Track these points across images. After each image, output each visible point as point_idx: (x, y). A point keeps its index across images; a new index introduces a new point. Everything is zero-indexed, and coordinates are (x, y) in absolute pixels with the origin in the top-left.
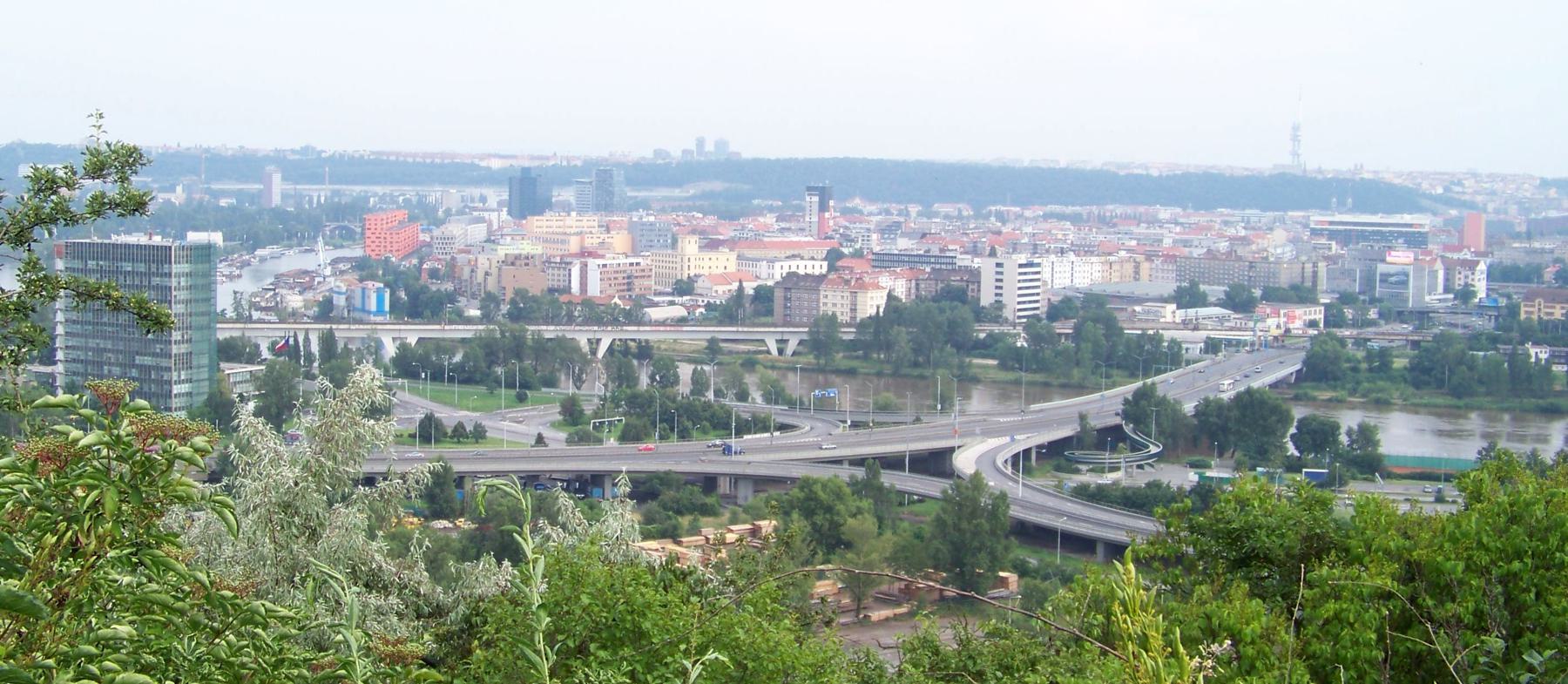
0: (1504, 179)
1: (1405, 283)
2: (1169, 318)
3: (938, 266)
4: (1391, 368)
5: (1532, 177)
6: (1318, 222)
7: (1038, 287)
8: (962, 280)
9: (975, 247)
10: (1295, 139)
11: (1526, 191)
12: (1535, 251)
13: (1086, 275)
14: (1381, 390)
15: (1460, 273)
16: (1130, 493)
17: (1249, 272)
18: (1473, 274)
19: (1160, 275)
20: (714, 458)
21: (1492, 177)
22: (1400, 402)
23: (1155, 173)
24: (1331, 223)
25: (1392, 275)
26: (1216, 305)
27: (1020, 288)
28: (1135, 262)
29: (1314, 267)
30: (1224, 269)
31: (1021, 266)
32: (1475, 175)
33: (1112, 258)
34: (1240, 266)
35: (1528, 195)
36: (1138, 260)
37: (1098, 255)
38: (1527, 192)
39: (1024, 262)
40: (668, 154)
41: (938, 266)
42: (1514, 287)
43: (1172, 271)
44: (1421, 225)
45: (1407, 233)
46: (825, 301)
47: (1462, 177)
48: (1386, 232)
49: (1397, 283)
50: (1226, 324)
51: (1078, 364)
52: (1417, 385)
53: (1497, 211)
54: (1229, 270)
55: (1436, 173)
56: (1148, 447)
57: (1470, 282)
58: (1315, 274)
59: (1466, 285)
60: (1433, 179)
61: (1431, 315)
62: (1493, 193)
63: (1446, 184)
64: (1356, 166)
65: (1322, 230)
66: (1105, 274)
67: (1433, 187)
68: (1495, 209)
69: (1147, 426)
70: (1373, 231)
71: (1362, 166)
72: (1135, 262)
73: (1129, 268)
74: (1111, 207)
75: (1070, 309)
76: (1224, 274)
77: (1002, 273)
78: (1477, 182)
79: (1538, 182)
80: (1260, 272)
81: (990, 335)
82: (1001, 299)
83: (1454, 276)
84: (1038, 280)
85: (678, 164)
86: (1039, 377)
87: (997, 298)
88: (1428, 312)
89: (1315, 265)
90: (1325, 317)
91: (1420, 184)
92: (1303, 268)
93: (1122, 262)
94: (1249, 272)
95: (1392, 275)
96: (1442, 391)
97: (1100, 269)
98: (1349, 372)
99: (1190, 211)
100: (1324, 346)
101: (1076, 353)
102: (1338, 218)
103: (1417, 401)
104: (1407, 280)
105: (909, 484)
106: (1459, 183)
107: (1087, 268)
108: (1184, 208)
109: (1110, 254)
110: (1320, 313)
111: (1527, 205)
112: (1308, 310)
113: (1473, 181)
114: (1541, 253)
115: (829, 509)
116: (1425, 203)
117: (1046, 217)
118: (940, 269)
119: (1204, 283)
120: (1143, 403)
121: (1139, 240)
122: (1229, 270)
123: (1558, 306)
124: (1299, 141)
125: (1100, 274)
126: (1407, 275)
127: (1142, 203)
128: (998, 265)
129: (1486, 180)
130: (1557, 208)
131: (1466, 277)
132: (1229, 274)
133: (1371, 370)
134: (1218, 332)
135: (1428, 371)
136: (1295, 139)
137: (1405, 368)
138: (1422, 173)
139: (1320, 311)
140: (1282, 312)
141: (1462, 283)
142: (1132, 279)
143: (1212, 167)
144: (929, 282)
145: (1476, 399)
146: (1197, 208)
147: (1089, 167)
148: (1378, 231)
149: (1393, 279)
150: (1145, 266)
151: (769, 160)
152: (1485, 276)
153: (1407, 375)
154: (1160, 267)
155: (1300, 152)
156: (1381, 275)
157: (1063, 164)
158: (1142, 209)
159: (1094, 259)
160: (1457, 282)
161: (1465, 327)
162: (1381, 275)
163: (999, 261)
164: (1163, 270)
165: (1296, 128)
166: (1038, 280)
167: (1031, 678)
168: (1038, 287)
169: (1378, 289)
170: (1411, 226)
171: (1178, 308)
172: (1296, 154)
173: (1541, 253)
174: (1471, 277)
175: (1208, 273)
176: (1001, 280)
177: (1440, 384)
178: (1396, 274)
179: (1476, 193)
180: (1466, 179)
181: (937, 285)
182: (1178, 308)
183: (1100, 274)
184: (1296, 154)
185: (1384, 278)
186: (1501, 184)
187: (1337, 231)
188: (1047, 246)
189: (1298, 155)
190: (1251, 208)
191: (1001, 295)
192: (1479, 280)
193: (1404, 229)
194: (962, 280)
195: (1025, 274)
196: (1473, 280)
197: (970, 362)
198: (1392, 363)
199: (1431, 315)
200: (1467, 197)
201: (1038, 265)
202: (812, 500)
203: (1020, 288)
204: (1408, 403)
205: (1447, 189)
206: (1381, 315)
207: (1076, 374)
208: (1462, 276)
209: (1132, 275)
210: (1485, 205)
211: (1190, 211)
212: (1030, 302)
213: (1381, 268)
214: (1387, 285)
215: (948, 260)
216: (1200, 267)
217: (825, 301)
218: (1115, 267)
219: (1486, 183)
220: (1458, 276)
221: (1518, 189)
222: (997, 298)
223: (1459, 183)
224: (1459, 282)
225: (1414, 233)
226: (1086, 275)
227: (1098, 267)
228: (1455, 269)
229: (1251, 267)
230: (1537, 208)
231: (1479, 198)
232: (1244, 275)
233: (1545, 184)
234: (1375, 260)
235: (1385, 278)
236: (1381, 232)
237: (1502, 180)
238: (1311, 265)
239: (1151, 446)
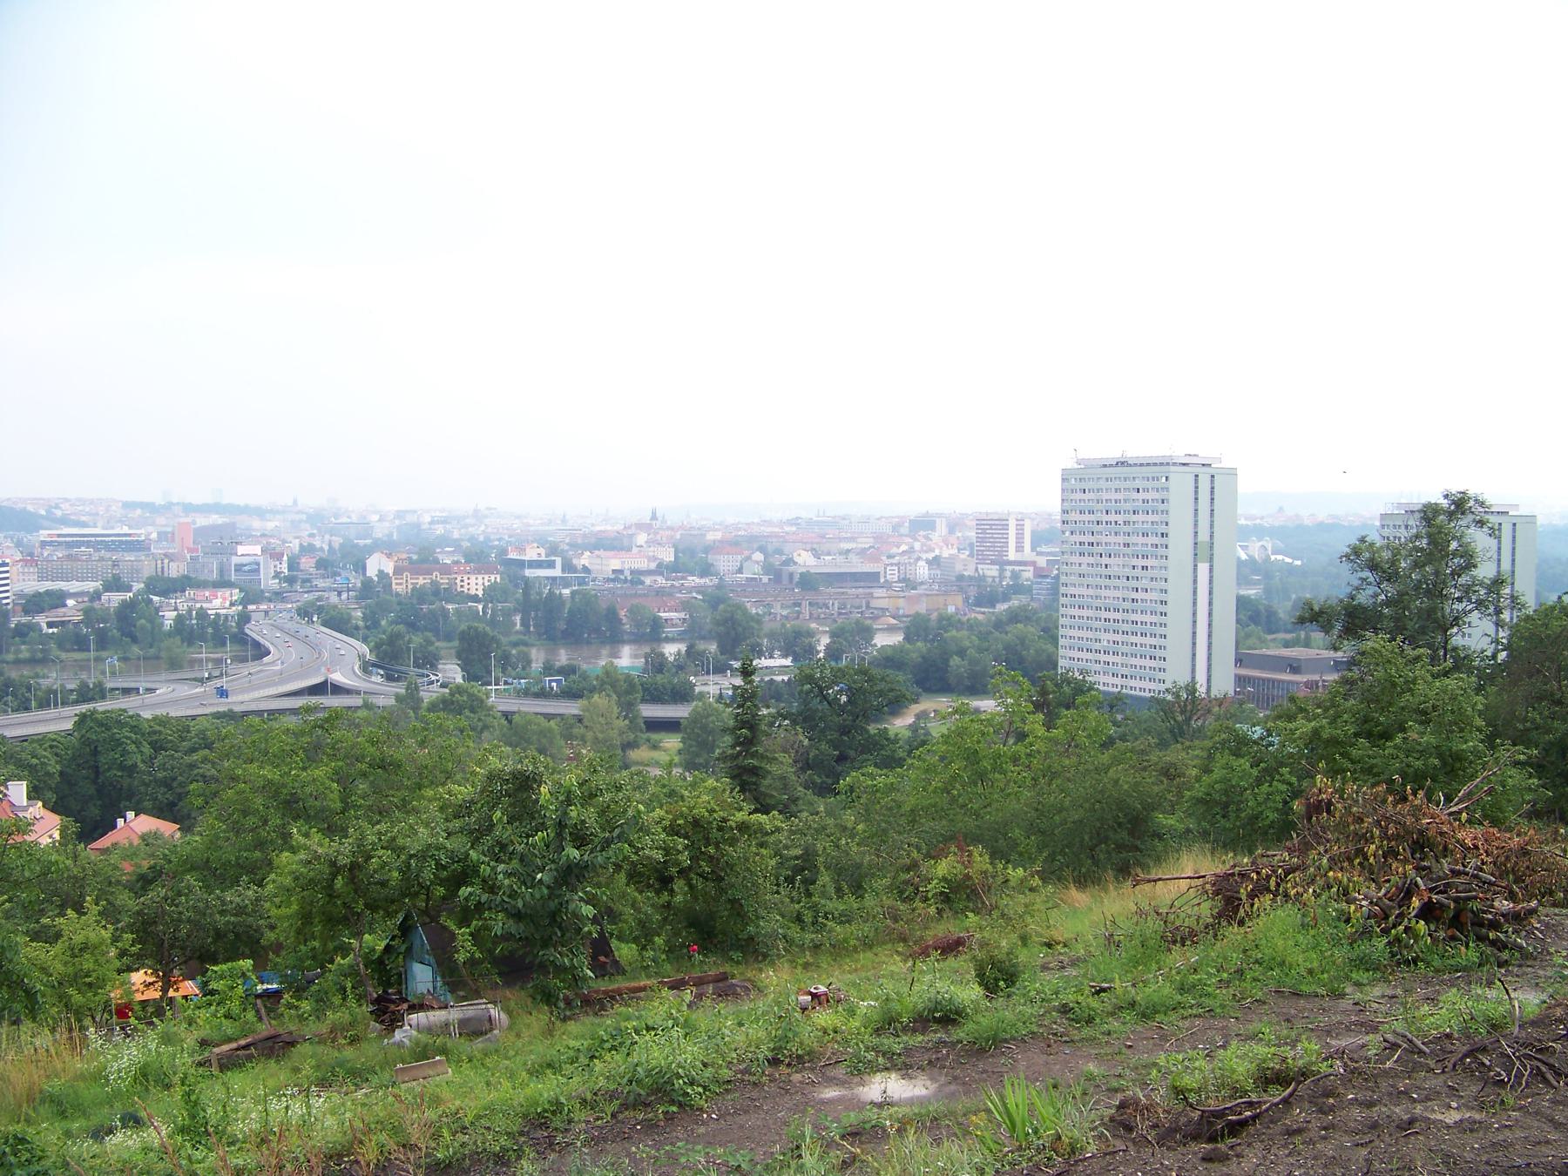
0: (92, 502)
1: (257, 571)
16: (890, 652)
19: (21, 577)
20: (212, 701)
24: (59, 536)
25: (245, 565)
32: (66, 500)
44: (139, 535)
45: (126, 541)
49: (249, 571)
54: (92, 569)
55: (29, 499)
58: (163, 568)
95: (245, 565)
106: (57, 507)
122: (92, 569)
123: (421, 578)
126: (258, 564)
132: (92, 573)
140: (219, 594)
149: (246, 568)
151: (238, 506)
154: (21, 570)
164: (23, 573)
167: (18, 1172)
170: (130, 535)
185: (238, 568)
193: (124, 539)
199: (529, 573)
213: (235, 560)
216: (62, 569)
233: (128, 506)
235: (239, 568)
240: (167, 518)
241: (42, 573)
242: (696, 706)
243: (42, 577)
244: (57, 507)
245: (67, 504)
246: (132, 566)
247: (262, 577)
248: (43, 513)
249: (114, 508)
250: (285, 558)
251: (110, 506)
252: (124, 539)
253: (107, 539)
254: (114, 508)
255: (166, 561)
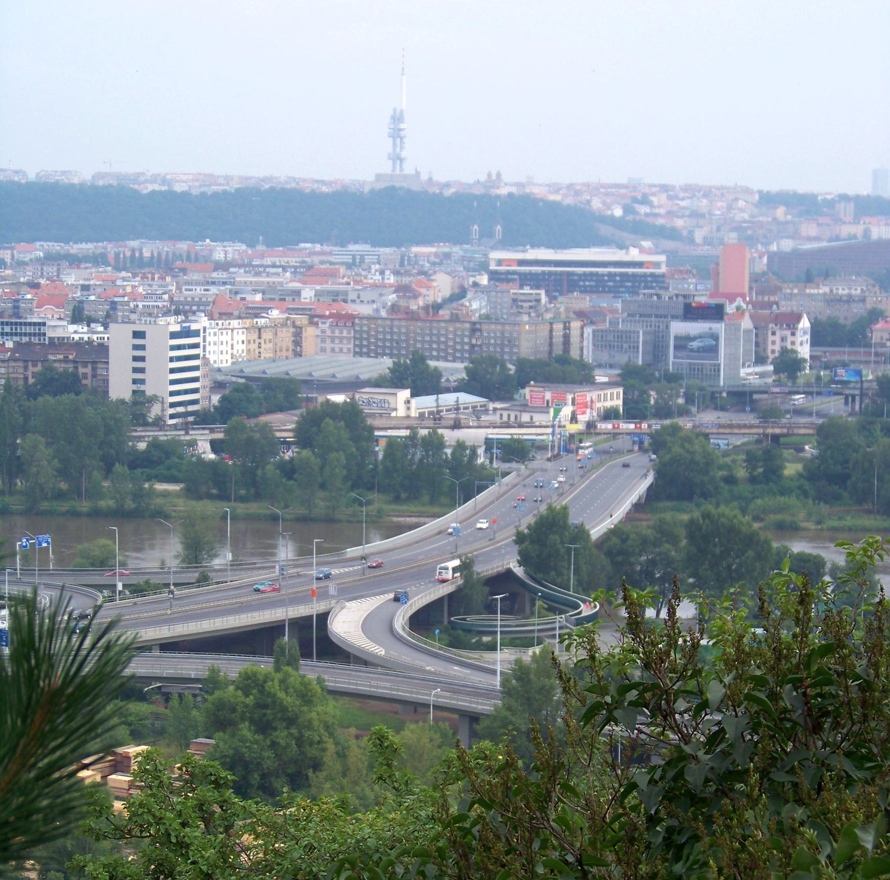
0: (707, 193)
1: (713, 350)
2: (401, 412)
3: (25, 339)
4: (780, 477)
5: (747, 191)
6: (500, 262)
7: (196, 368)
8: (66, 360)
9: (16, 307)
10: (397, 134)
11: (742, 210)
12: (839, 300)
13: (223, 348)
14: (781, 510)
15: (774, 334)
17: (470, 337)
18: (793, 334)
19: (328, 345)
21: (691, 190)
22: (812, 526)
23: (179, 188)
24: (521, 263)
25: (694, 339)
26: (456, 390)
27: (172, 371)
28: (294, 326)
29: (565, 328)
30: (431, 335)
31: (174, 335)
32: (665, 188)
33: (261, 322)
34: (456, 330)
35: (746, 216)
36: (298, 323)
37: (240, 318)
38: (743, 213)
39: (177, 328)
40: (25, 174)
41: (25, 339)
42: (850, 353)
43: (348, 339)
45: (634, 275)
46: (224, 362)
47: (647, 191)
48: (603, 275)
50: (484, 418)
51: (323, 486)
52: (821, 497)
53: (707, 241)
55: (603, 186)
56: (577, 606)
57: (789, 347)
58: (567, 338)
59: (784, 351)
60: (606, 194)
61: (755, 396)
62: (696, 215)
63: (628, 201)
64: (489, 175)
65: (508, 273)
66: (254, 346)
67: (608, 206)
68: (705, 238)
69: (560, 574)
70: (585, 274)
71: (499, 175)
72: (294, 326)
73: (286, 336)
74: (134, 244)
75: (249, 401)
76: (431, 342)
77: (142, 347)
78: (670, 198)
79: (757, 197)
80: (489, 338)
81: (155, 444)
82: (142, 388)
83: (765, 341)
84: (196, 357)
85: (372, 192)
86: (254, 508)
87: (135, 387)
88: (751, 393)
89: (566, 327)
90: (624, 403)
91: (589, 202)
92: (551, 331)
93: (275, 326)
94: (470, 337)
96: (867, 506)
97: (244, 338)
98: (722, 484)
99: (261, 248)
100: (686, 445)
101: (322, 468)
102: (533, 254)
103: (835, 523)
104: (717, 345)
105: (59, 673)
106: (645, 201)
107: (226, 337)
108: (251, 245)
109: (257, 316)
110: (618, 398)
111: (749, 232)
112: (602, 393)
113: (663, 197)
114: (848, 302)
115: (291, 721)
116: (605, 230)
117: (50, 258)
118: (29, 344)
119: (433, 358)
120: (554, 538)
121: (264, 293)
124: (402, 138)
125: (244, 347)
126: (716, 338)
127: (180, 238)
128: (138, 335)
129: (681, 195)
130: (795, 235)
131: (783, 339)
133: (753, 480)
134: (496, 430)
135: (841, 479)
136: (397, 134)
137: (800, 476)
138: (588, 185)
139: (618, 394)
140: (570, 397)
141: (777, 348)
142: (290, 354)
143: (263, 180)
144: (12, 364)
145: (267, 512)
146: (270, 244)
147: (76, 181)
148: (592, 274)
149: (695, 344)
150: (310, 333)
152: (808, 337)
153: (807, 485)
154: (329, 333)
155: (404, 154)
156: (677, 338)
157: (32, 176)
158: (183, 246)
159: (235, 323)
160: (770, 347)
161: (819, 414)
162: (677, 338)
163: (138, 328)
164: (333, 339)
165: (397, 118)
166: (196, 357)
168: (196, 368)
169: (671, 359)
170: (640, 264)
171: (413, 395)
172: (396, 159)
173: (848, 302)
174: (790, 339)
175: (407, 341)
176: (142, 359)
177: (862, 497)
178: (700, 337)
179: (670, 214)
180: (654, 194)
181: (26, 368)
182: (413, 395)
183: (244, 347)
184: (396, 159)
186: (705, 201)
187: (530, 273)
188: (132, 305)
189: (401, 160)
190: (356, 242)
191: (142, 382)
192: (801, 344)
193: (630, 270)
194: (66, 360)
195: (179, 347)
196: (793, 343)
197: (151, 487)
198: (784, 468)
199: (755, 396)
200: (660, 221)
201: (196, 333)
202: (266, 706)
203: (172, 371)
204: (825, 526)
205: (627, 210)
206: (689, 399)
207: (321, 503)
208: (777, 338)
209: (291, 347)
210: (691, 232)
211: (261, 248)
212: (186, 392)
214: (685, 354)
215: (31, 330)
216: (392, 333)
217: (224, 362)
218: (267, 335)
219: (683, 199)
220: (771, 338)
221: (730, 208)
222: (135, 387)
223: (645, 200)
224: (774, 346)
225: (645, 275)
226: (223, 348)
227: (241, 336)
228: (766, 328)
229: (473, 331)
230: (765, 237)
231: (679, 223)
232: (462, 343)
233: (768, 200)
234: (666, 316)
236: (597, 274)
237: (705, 196)
238: (561, 326)
239: (583, 606)
240: (819, 225)
241: (361, 339)
242: (534, 653)
243: (361, 346)
244: (645, 201)
245: (663, 197)
246: (502, 333)
247: (722, 361)
248: (618, 212)
249: (741, 204)
250: (805, 323)
251: (736, 200)
252: (630, 270)
253: (600, 270)
254: (741, 204)
255: (575, 325)
